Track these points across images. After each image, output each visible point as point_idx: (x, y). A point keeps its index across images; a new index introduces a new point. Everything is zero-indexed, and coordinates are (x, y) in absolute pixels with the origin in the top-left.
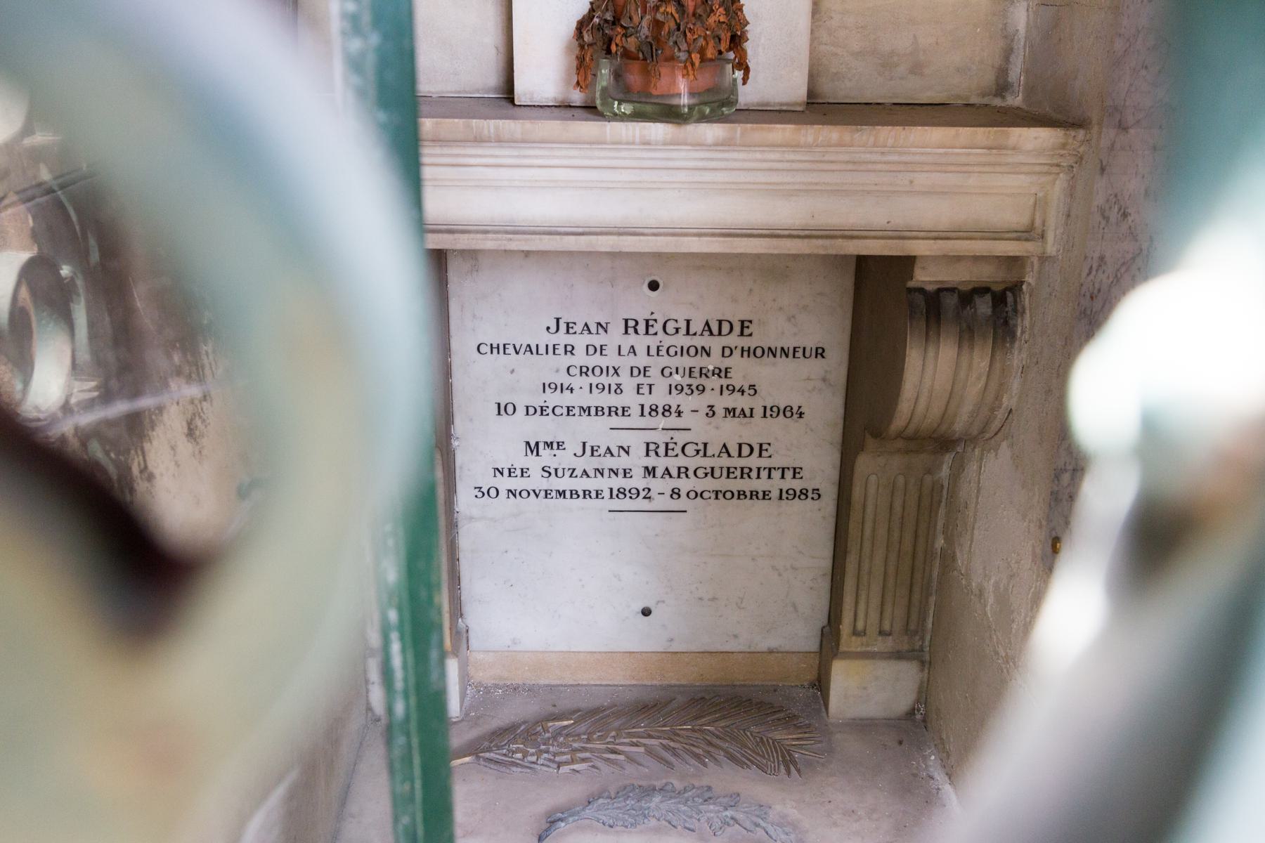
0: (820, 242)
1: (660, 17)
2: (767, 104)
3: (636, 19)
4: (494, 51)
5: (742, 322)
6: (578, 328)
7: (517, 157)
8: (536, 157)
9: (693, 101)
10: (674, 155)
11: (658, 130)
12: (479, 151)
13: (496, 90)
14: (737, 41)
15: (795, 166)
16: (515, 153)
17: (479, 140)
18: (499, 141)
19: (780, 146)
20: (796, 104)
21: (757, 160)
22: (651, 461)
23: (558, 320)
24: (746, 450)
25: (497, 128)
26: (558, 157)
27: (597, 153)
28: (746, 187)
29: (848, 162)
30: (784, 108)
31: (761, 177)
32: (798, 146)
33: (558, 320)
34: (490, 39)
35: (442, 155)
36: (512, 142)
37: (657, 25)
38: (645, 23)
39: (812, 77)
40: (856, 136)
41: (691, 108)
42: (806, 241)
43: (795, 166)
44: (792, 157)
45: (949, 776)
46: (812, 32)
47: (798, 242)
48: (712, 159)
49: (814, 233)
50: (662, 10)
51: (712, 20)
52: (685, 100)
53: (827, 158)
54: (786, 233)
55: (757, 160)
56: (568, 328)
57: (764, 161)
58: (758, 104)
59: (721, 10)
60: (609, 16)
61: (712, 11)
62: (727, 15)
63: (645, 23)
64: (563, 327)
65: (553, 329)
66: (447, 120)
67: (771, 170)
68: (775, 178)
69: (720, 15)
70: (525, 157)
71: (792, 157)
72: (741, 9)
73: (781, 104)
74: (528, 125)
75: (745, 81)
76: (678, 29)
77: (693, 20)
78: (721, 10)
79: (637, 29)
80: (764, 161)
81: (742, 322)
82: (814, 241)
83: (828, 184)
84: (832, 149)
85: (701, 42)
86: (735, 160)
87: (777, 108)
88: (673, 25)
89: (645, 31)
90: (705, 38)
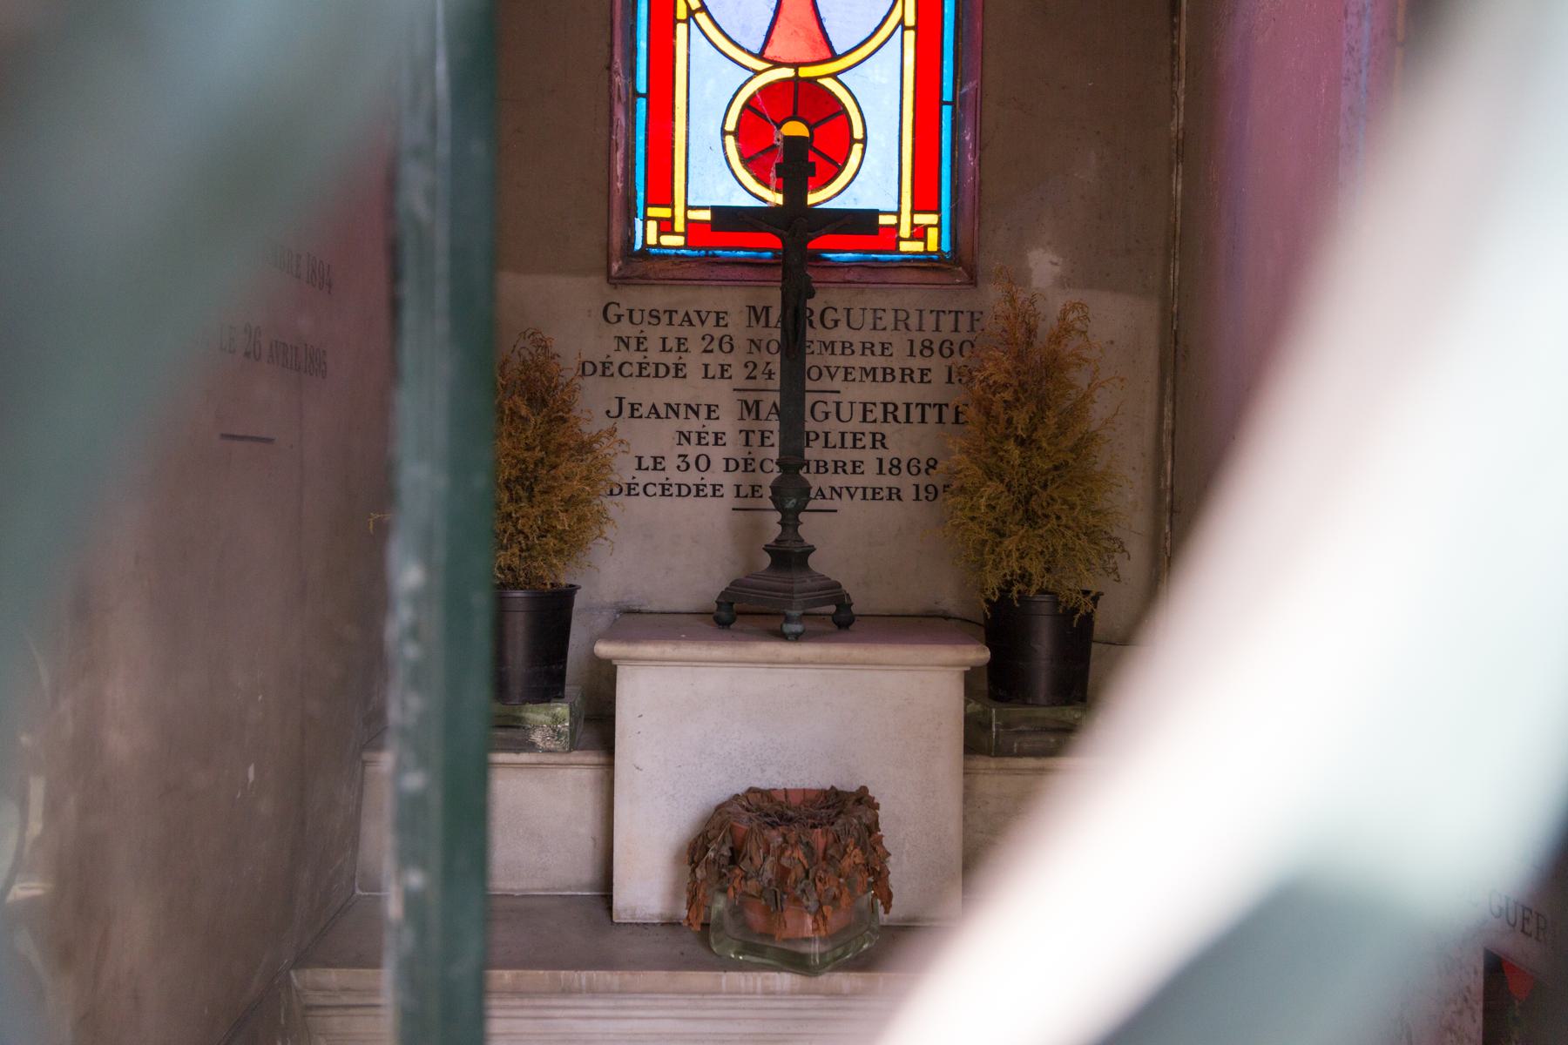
1: (785, 862)
3: (758, 861)
4: (590, 843)
5: (865, 405)
6: (644, 410)
7: (614, 1008)
8: (637, 1008)
9: (824, 949)
10: (804, 1004)
11: (784, 980)
12: (568, 1002)
13: (591, 887)
16: (612, 1003)
17: (567, 991)
18: (593, 992)
23: (621, 399)
24: (684, 491)
25: (589, 980)
26: (662, 1008)
27: (710, 1004)
33: (621, 399)
34: (585, 830)
35: (522, 1007)
36: (608, 992)
37: (783, 873)
38: (768, 866)
41: (822, 955)
46: (965, 818)
50: (788, 853)
51: (846, 863)
52: (815, 949)
56: (633, 410)
58: (904, 920)
60: (726, 852)
63: (768, 866)
64: (627, 410)
65: (615, 412)
66: (530, 972)
69: (856, 856)
70: (623, 1008)
72: (879, 841)
74: (627, 976)
75: (887, 912)
76: (807, 876)
77: (823, 864)
79: (758, 874)
81: (865, 405)
85: (835, 890)
88: (800, 870)
89: (768, 872)
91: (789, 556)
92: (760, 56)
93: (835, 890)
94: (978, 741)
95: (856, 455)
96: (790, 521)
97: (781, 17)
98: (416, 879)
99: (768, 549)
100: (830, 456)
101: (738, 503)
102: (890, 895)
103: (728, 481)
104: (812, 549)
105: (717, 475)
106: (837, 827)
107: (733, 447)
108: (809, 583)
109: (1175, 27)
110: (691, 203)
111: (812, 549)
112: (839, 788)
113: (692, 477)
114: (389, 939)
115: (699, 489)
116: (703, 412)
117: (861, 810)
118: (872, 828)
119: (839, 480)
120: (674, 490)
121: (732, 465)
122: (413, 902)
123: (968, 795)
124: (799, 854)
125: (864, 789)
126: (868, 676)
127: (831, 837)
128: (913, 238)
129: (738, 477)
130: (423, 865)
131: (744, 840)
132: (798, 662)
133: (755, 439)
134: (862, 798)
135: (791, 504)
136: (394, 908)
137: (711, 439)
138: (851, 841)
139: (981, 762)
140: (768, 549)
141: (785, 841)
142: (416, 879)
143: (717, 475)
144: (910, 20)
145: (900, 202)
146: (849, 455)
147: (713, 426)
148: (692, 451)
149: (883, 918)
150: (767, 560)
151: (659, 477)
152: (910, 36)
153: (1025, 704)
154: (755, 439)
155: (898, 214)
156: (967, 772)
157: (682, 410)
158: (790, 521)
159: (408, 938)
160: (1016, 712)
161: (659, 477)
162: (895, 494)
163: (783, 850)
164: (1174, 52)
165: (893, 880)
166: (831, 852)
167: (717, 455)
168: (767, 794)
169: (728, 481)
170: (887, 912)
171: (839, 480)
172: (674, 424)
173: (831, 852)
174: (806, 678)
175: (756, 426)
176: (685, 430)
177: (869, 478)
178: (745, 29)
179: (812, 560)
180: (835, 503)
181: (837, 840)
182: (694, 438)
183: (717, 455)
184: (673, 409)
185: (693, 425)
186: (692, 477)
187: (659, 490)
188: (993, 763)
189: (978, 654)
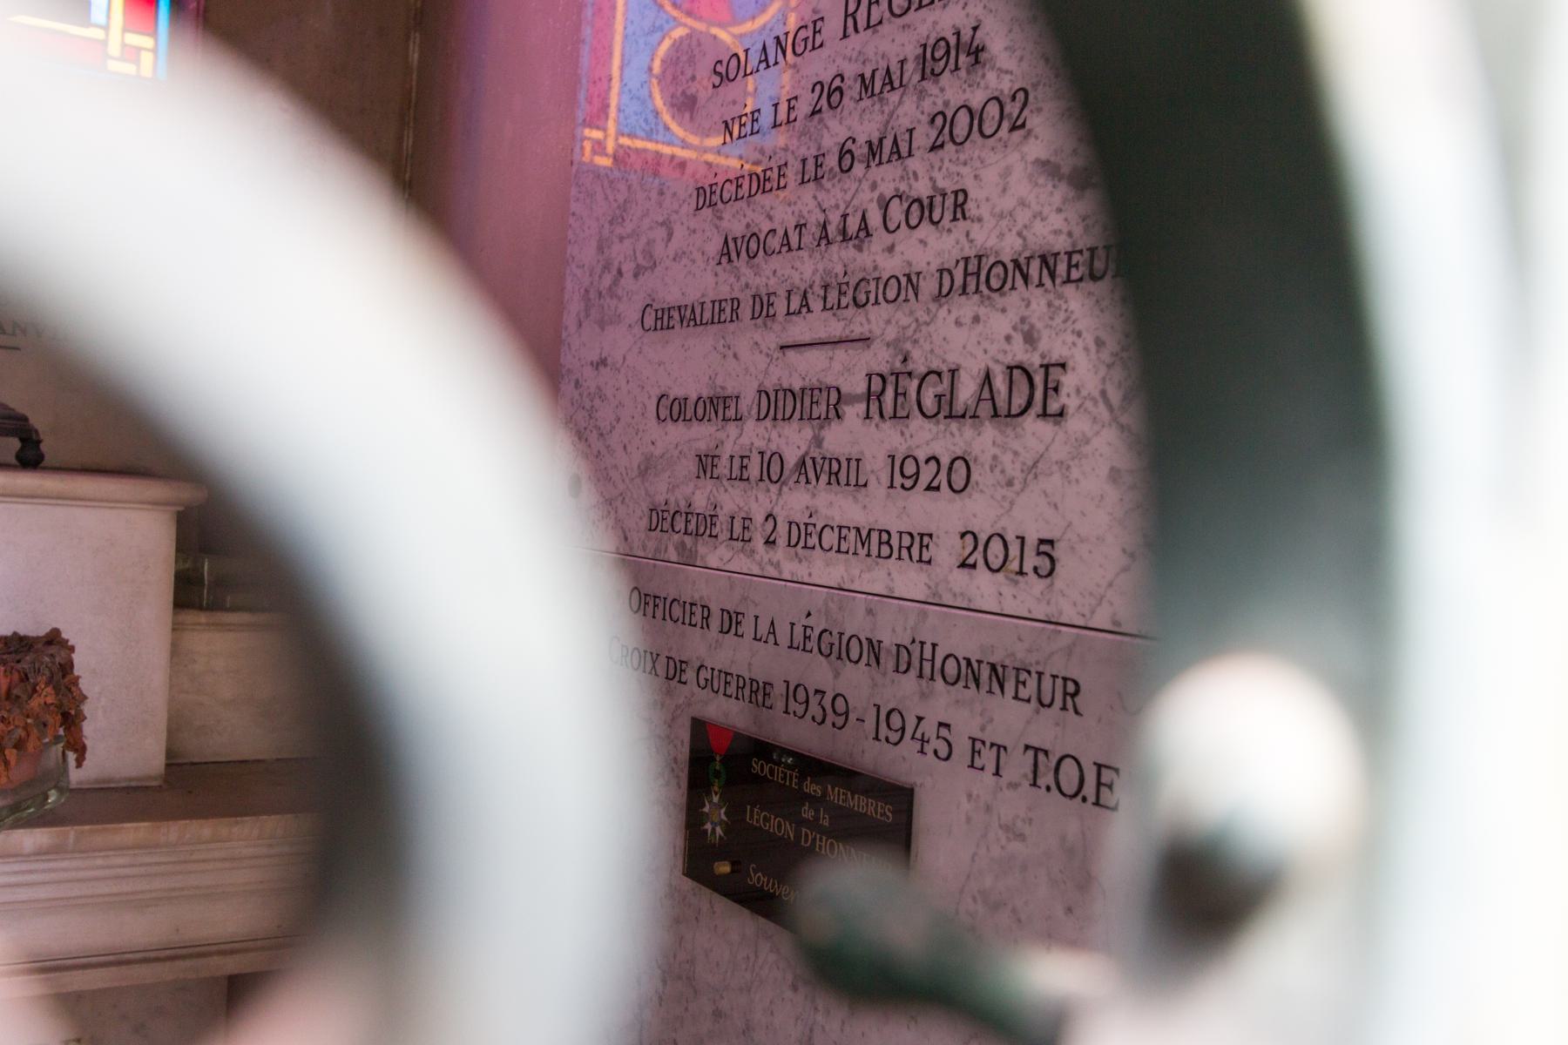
0: (188, 963)
2: (110, 780)
14: (71, 719)
15: (155, 869)
19: (128, 848)
20: (150, 778)
21: (99, 868)
22: (759, 542)
28: (80, 901)
29: (224, 860)
30: (133, 784)
31: (103, 888)
32: (157, 846)
39: (172, 733)
40: (235, 830)
42: (168, 964)
43: (155, 869)
44: (148, 859)
45: (79, 997)
47: (158, 967)
48: (31, 872)
49: (179, 952)
51: (35, 703)
53: (194, 857)
54: (138, 956)
55: (99, 868)
57: (109, 867)
58: (97, 781)
59: (49, 689)
61: (35, 691)
62: (57, 689)
67: (117, 877)
68: (126, 887)
69: (47, 695)
71: (148, 859)
73: (131, 780)
75: (79, 764)
78: (49, 689)
80: (109, 867)
82: (180, 964)
83: (197, 887)
84: (203, 847)
85: (20, 732)
86: (64, 870)
87: (124, 784)
90: (26, 727)
93: (20, 732)
102: (84, 748)
106: (24, 665)
110: (1051, 370)
112: (22, 632)
117: (53, 650)
118: (67, 668)
123: (175, 651)
126: (60, 513)
127: (16, 676)
128: (137, 62)
134: (54, 639)
138: (42, 680)
139: (190, 617)
145: (108, 17)
149: (76, 776)
155: (106, 28)
156: (177, 628)
165: (88, 728)
166: (15, 692)
170: (79, 764)
173: (15, 692)
181: (25, 678)
188: (203, 618)
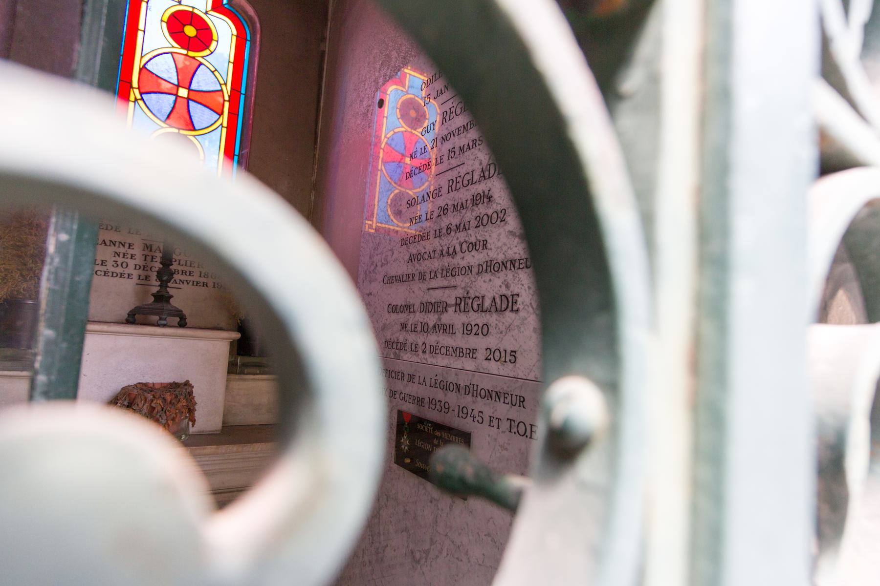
1: (153, 405)
3: (141, 405)
24: (115, 275)
51: (179, 405)
69: (184, 402)
85: (173, 415)
88: (160, 409)
91: (162, 298)
92: (201, 64)
94: (233, 369)
95: (191, 269)
96: (164, 284)
97: (175, 111)
98: (64, 237)
99: (153, 295)
100: (180, 268)
101: (139, 282)
103: (135, 273)
104: (171, 297)
105: (131, 270)
107: (139, 260)
108: (170, 308)
109: (315, 148)
111: (171, 297)
113: (119, 270)
114: (48, 260)
115: (122, 275)
116: (127, 246)
118: (191, 393)
119: (183, 277)
120: (110, 274)
121: (138, 267)
122: (60, 246)
123: (227, 388)
124: (160, 401)
125: (188, 381)
126: (191, 342)
129: (140, 272)
130: (69, 232)
131: (135, 398)
132: (164, 335)
133: (149, 259)
135: (165, 278)
136: (51, 248)
137: (129, 256)
138: (182, 397)
139: (233, 376)
140: (153, 295)
141: (154, 397)
142: (64, 237)
143: (131, 270)
144: (225, 124)
146: (188, 269)
147: (130, 252)
148: (120, 260)
149: (192, 430)
150: (152, 299)
151: (104, 268)
152: (224, 130)
153: (250, 356)
154: (149, 259)
156: (228, 380)
157: (117, 244)
158: (164, 284)
159: (57, 260)
160: (247, 359)
161: (104, 268)
162: (205, 285)
163: (152, 401)
164: (315, 155)
165: (197, 414)
167: (132, 263)
168: (146, 385)
169: (135, 273)
171: (183, 277)
172: (113, 249)
174: (166, 342)
175: (150, 253)
176: (118, 251)
177: (196, 278)
178: (159, 111)
179: (172, 300)
180: (181, 286)
181: (176, 397)
182: (121, 255)
183: (132, 263)
184: (113, 243)
185: (122, 250)
186: (119, 270)
187: (103, 273)
188: (237, 377)
189: (236, 335)
